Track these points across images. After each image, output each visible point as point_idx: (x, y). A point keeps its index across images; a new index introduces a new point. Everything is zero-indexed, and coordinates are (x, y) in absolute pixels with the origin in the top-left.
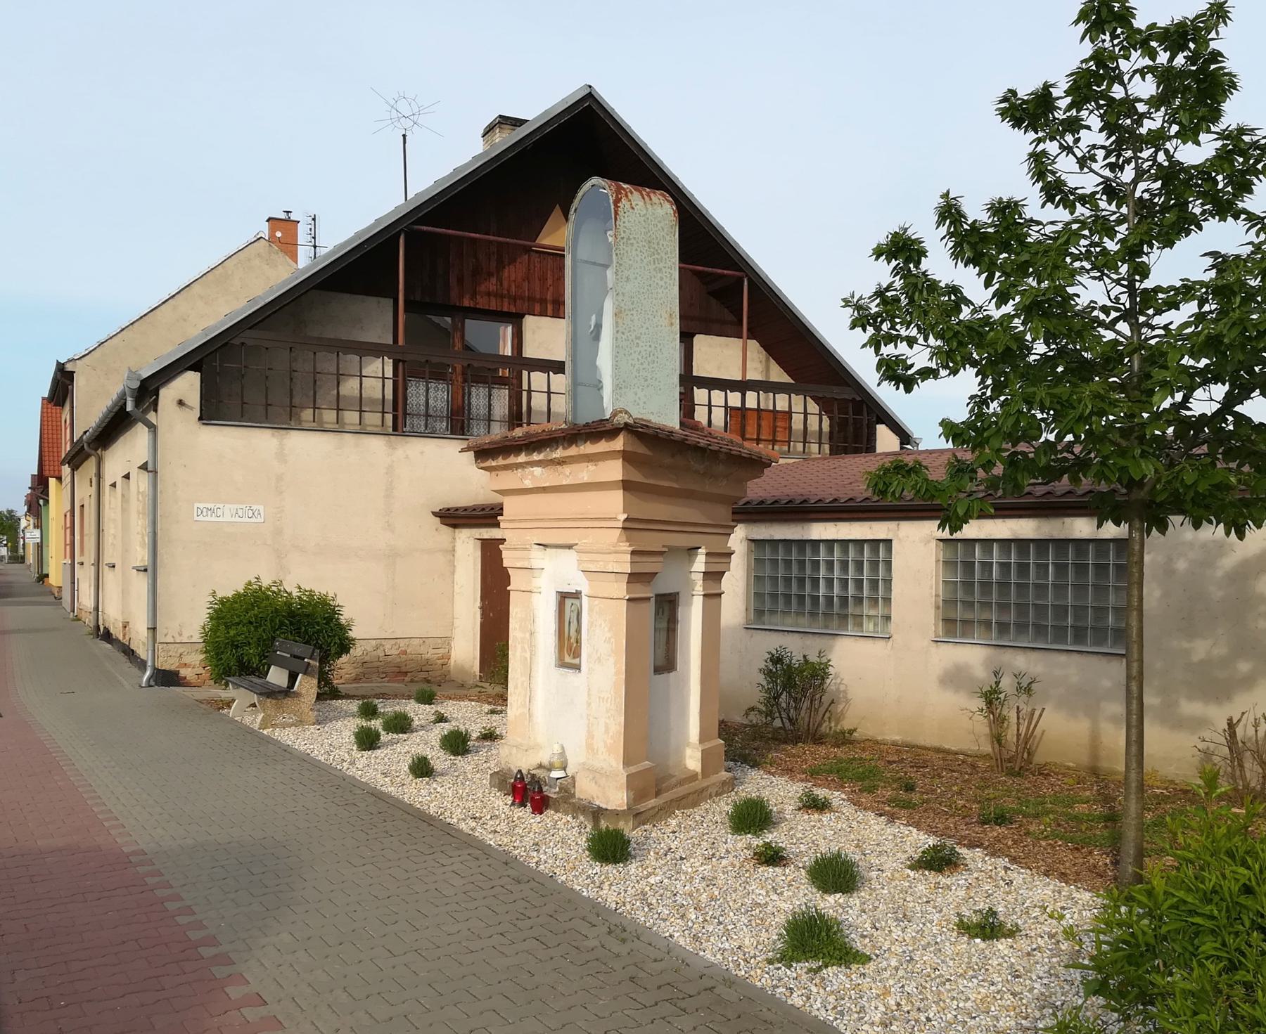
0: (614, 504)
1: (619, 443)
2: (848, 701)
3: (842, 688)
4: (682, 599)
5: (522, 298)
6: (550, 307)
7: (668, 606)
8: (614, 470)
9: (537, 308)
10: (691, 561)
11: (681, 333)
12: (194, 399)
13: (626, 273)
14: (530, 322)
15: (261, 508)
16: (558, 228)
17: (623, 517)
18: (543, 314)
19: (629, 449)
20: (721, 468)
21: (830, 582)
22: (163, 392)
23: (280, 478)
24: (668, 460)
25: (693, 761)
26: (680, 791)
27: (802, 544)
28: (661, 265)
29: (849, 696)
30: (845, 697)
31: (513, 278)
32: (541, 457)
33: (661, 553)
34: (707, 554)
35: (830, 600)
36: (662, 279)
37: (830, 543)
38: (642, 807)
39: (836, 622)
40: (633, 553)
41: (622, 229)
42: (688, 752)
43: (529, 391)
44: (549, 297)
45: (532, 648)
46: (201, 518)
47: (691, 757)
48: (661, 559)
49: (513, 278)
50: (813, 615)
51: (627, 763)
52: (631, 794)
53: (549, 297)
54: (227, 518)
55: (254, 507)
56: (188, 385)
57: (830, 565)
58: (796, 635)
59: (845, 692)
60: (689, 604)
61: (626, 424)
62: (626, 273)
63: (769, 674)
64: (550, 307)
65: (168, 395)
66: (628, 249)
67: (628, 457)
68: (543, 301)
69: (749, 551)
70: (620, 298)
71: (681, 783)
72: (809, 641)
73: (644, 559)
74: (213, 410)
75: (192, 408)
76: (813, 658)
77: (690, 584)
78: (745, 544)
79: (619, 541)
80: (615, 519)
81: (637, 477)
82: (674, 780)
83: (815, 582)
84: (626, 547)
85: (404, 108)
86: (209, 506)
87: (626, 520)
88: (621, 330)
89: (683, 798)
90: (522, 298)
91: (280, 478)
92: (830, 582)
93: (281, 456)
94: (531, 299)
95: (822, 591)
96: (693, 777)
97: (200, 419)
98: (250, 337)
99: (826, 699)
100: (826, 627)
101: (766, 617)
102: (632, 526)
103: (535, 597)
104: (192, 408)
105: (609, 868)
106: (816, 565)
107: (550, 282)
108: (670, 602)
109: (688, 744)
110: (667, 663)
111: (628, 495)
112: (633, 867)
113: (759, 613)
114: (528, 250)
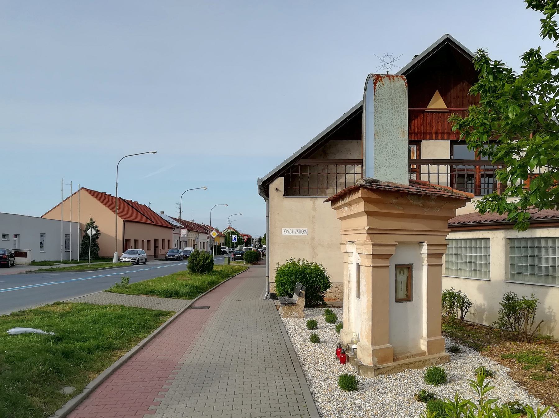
0: (363, 222)
1: (358, 195)
2: (555, 321)
3: (553, 314)
4: (414, 267)
5: (421, 133)
6: (434, 136)
7: (406, 269)
8: (360, 207)
9: (428, 137)
10: (421, 248)
11: (409, 141)
12: (282, 188)
13: (380, 115)
14: (424, 143)
15: (307, 229)
16: (437, 101)
17: (367, 228)
18: (431, 139)
19: (366, 196)
20: (433, 203)
21: (547, 259)
22: (270, 186)
23: (314, 217)
24: (394, 201)
25: (424, 346)
26: (405, 361)
27: (533, 239)
28: (398, 109)
29: (556, 318)
30: (554, 319)
31: (416, 125)
32: (343, 202)
33: (395, 245)
34: (428, 245)
35: (547, 268)
36: (399, 116)
37: (547, 239)
38: (381, 366)
39: (550, 279)
40: (373, 245)
41: (377, 95)
42: (422, 341)
43: (447, 174)
44: (433, 131)
45: (349, 288)
46: (284, 234)
47: (423, 344)
48: (394, 248)
49: (416, 125)
50: (539, 276)
51: (374, 343)
52: (376, 359)
53: (433, 131)
54: (294, 234)
55: (304, 229)
56: (280, 182)
57: (547, 249)
58: (529, 286)
59: (554, 316)
60: (420, 269)
61: (361, 185)
62: (380, 115)
63: (505, 306)
64: (434, 136)
65: (272, 187)
66: (381, 104)
67: (367, 200)
68: (430, 134)
69: (507, 244)
70: (377, 126)
71: (413, 356)
72: (536, 289)
73: (382, 248)
74: (289, 191)
75: (281, 191)
76: (528, 298)
77: (421, 260)
78: (504, 240)
79: (367, 239)
80: (364, 229)
81: (373, 208)
82: (409, 354)
83: (540, 259)
84: (369, 242)
85: (387, 60)
86: (287, 229)
87: (369, 229)
88: (377, 141)
89: (411, 363)
90: (421, 133)
91: (314, 217)
92: (547, 259)
93: (314, 208)
94: (425, 133)
95: (543, 263)
96: (423, 354)
97: (284, 195)
98: (303, 162)
99: (537, 320)
100: (546, 282)
101: (516, 277)
102: (371, 232)
103: (350, 265)
104: (281, 191)
105: (345, 393)
106: (540, 250)
107: (434, 124)
108: (408, 268)
109: (422, 337)
110: (406, 296)
111: (371, 218)
112: (355, 394)
113: (513, 274)
114: (423, 112)
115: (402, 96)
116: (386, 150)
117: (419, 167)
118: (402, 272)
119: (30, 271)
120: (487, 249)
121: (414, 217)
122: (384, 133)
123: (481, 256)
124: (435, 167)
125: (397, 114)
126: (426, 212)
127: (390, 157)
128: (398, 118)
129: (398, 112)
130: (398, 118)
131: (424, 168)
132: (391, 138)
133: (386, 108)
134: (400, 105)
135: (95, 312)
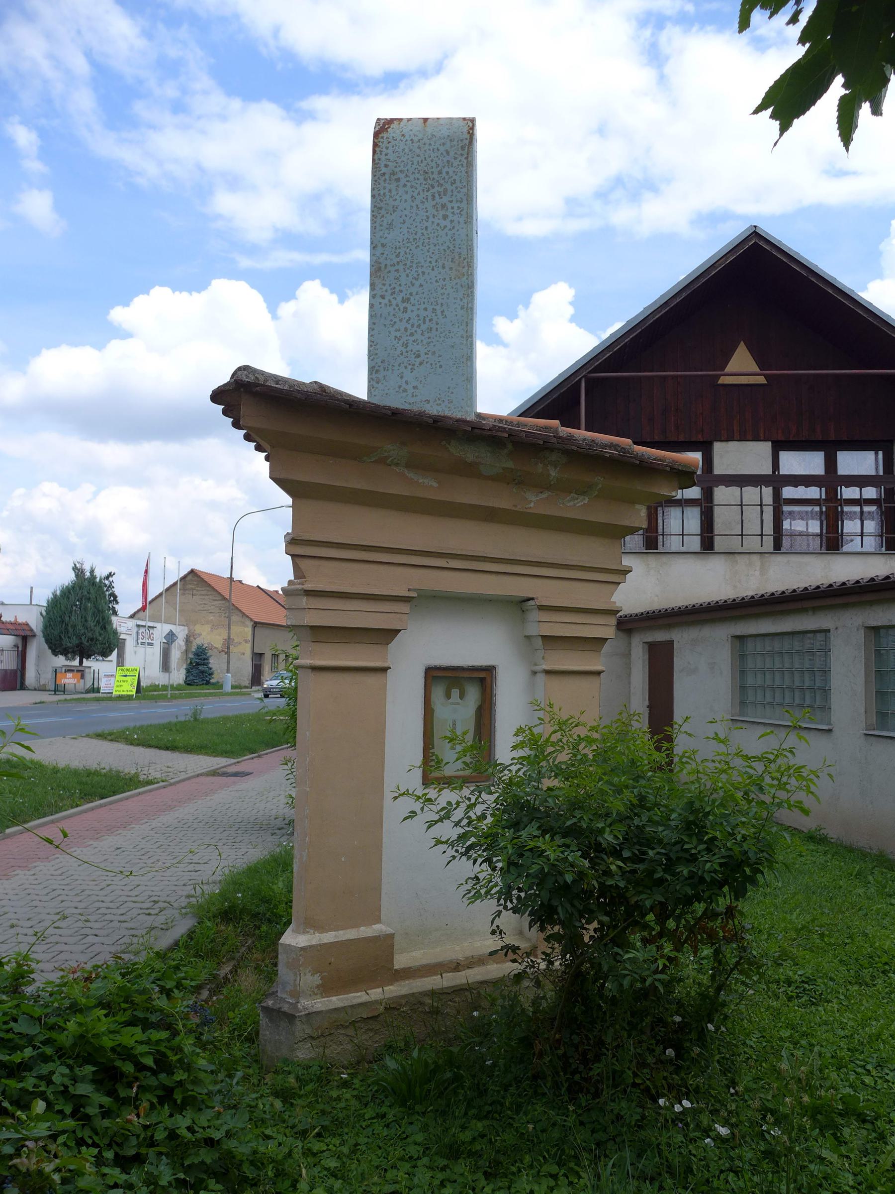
14: (718, 447)
28: (445, 200)
36: (445, 217)
70: (380, 249)
108: (482, 681)
115: (456, 163)
116: (406, 316)
117: (708, 495)
118: (455, 693)
119: (66, 700)
120: (826, 651)
121: (490, 515)
122: (401, 267)
123: (813, 672)
124: (735, 490)
125: (442, 213)
126: (534, 502)
127: (417, 336)
128: (443, 223)
129: (443, 206)
130: (443, 223)
131: (721, 494)
132: (421, 280)
133: (408, 197)
134: (449, 187)
135: (96, 779)
